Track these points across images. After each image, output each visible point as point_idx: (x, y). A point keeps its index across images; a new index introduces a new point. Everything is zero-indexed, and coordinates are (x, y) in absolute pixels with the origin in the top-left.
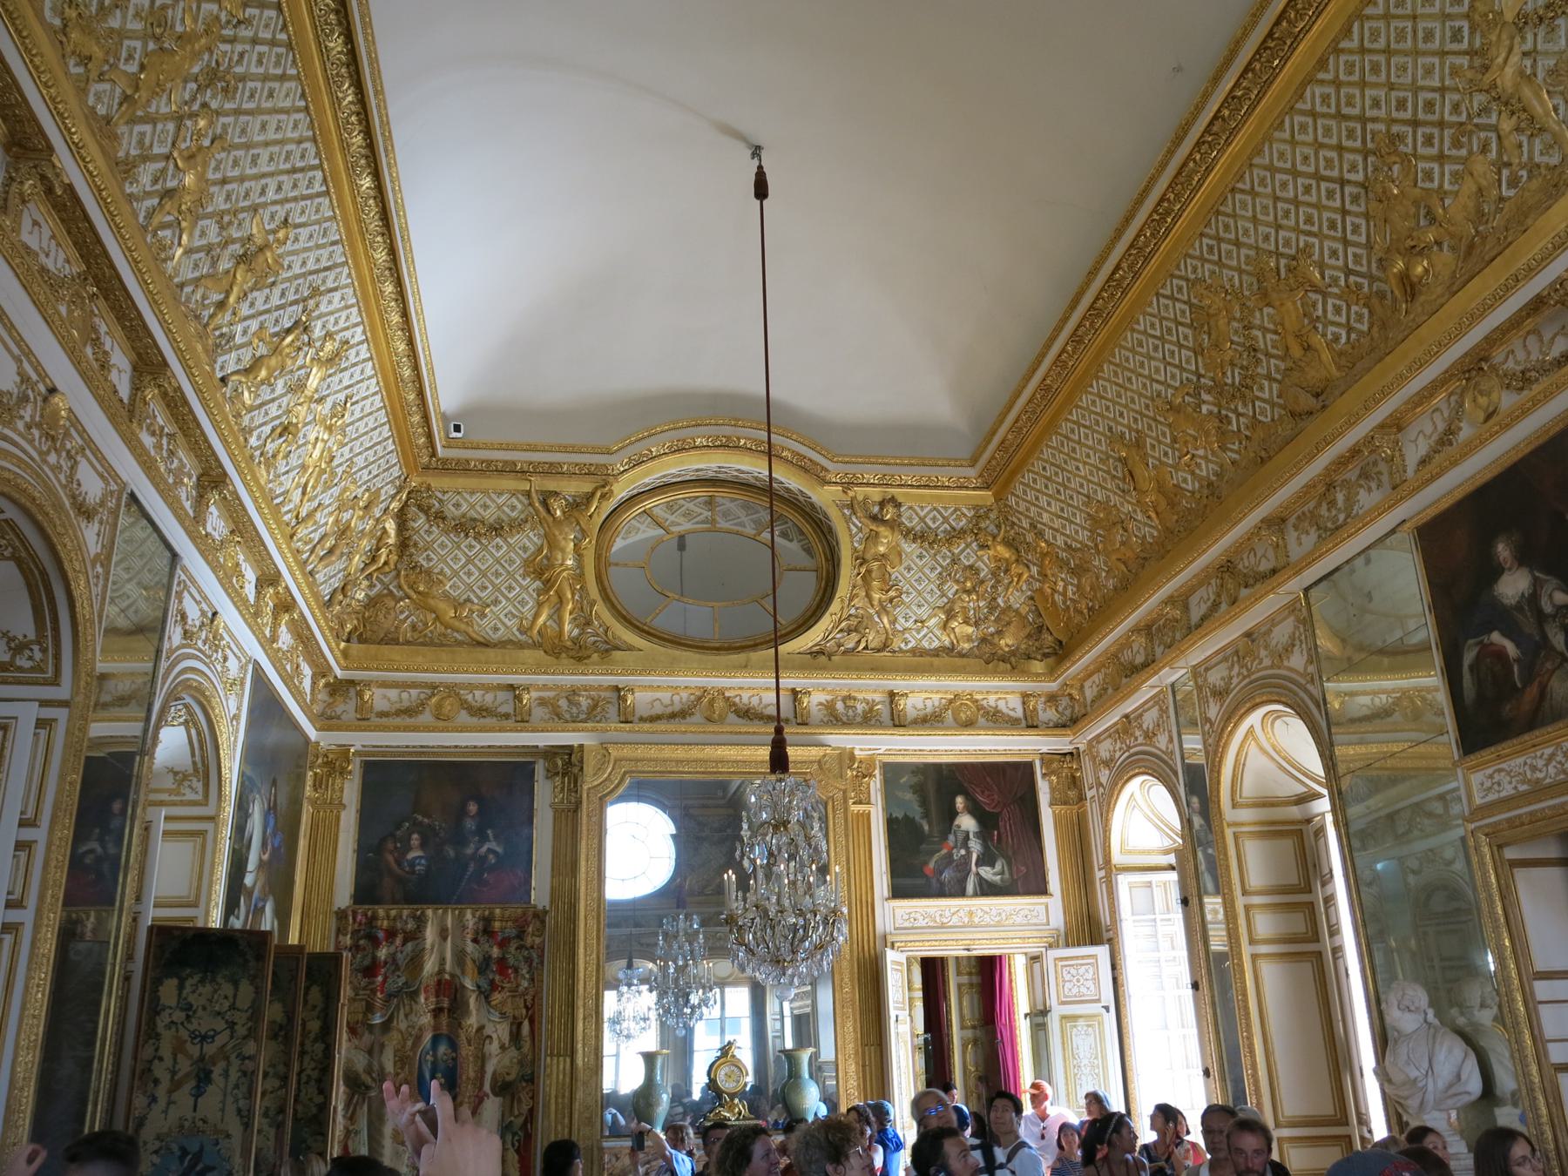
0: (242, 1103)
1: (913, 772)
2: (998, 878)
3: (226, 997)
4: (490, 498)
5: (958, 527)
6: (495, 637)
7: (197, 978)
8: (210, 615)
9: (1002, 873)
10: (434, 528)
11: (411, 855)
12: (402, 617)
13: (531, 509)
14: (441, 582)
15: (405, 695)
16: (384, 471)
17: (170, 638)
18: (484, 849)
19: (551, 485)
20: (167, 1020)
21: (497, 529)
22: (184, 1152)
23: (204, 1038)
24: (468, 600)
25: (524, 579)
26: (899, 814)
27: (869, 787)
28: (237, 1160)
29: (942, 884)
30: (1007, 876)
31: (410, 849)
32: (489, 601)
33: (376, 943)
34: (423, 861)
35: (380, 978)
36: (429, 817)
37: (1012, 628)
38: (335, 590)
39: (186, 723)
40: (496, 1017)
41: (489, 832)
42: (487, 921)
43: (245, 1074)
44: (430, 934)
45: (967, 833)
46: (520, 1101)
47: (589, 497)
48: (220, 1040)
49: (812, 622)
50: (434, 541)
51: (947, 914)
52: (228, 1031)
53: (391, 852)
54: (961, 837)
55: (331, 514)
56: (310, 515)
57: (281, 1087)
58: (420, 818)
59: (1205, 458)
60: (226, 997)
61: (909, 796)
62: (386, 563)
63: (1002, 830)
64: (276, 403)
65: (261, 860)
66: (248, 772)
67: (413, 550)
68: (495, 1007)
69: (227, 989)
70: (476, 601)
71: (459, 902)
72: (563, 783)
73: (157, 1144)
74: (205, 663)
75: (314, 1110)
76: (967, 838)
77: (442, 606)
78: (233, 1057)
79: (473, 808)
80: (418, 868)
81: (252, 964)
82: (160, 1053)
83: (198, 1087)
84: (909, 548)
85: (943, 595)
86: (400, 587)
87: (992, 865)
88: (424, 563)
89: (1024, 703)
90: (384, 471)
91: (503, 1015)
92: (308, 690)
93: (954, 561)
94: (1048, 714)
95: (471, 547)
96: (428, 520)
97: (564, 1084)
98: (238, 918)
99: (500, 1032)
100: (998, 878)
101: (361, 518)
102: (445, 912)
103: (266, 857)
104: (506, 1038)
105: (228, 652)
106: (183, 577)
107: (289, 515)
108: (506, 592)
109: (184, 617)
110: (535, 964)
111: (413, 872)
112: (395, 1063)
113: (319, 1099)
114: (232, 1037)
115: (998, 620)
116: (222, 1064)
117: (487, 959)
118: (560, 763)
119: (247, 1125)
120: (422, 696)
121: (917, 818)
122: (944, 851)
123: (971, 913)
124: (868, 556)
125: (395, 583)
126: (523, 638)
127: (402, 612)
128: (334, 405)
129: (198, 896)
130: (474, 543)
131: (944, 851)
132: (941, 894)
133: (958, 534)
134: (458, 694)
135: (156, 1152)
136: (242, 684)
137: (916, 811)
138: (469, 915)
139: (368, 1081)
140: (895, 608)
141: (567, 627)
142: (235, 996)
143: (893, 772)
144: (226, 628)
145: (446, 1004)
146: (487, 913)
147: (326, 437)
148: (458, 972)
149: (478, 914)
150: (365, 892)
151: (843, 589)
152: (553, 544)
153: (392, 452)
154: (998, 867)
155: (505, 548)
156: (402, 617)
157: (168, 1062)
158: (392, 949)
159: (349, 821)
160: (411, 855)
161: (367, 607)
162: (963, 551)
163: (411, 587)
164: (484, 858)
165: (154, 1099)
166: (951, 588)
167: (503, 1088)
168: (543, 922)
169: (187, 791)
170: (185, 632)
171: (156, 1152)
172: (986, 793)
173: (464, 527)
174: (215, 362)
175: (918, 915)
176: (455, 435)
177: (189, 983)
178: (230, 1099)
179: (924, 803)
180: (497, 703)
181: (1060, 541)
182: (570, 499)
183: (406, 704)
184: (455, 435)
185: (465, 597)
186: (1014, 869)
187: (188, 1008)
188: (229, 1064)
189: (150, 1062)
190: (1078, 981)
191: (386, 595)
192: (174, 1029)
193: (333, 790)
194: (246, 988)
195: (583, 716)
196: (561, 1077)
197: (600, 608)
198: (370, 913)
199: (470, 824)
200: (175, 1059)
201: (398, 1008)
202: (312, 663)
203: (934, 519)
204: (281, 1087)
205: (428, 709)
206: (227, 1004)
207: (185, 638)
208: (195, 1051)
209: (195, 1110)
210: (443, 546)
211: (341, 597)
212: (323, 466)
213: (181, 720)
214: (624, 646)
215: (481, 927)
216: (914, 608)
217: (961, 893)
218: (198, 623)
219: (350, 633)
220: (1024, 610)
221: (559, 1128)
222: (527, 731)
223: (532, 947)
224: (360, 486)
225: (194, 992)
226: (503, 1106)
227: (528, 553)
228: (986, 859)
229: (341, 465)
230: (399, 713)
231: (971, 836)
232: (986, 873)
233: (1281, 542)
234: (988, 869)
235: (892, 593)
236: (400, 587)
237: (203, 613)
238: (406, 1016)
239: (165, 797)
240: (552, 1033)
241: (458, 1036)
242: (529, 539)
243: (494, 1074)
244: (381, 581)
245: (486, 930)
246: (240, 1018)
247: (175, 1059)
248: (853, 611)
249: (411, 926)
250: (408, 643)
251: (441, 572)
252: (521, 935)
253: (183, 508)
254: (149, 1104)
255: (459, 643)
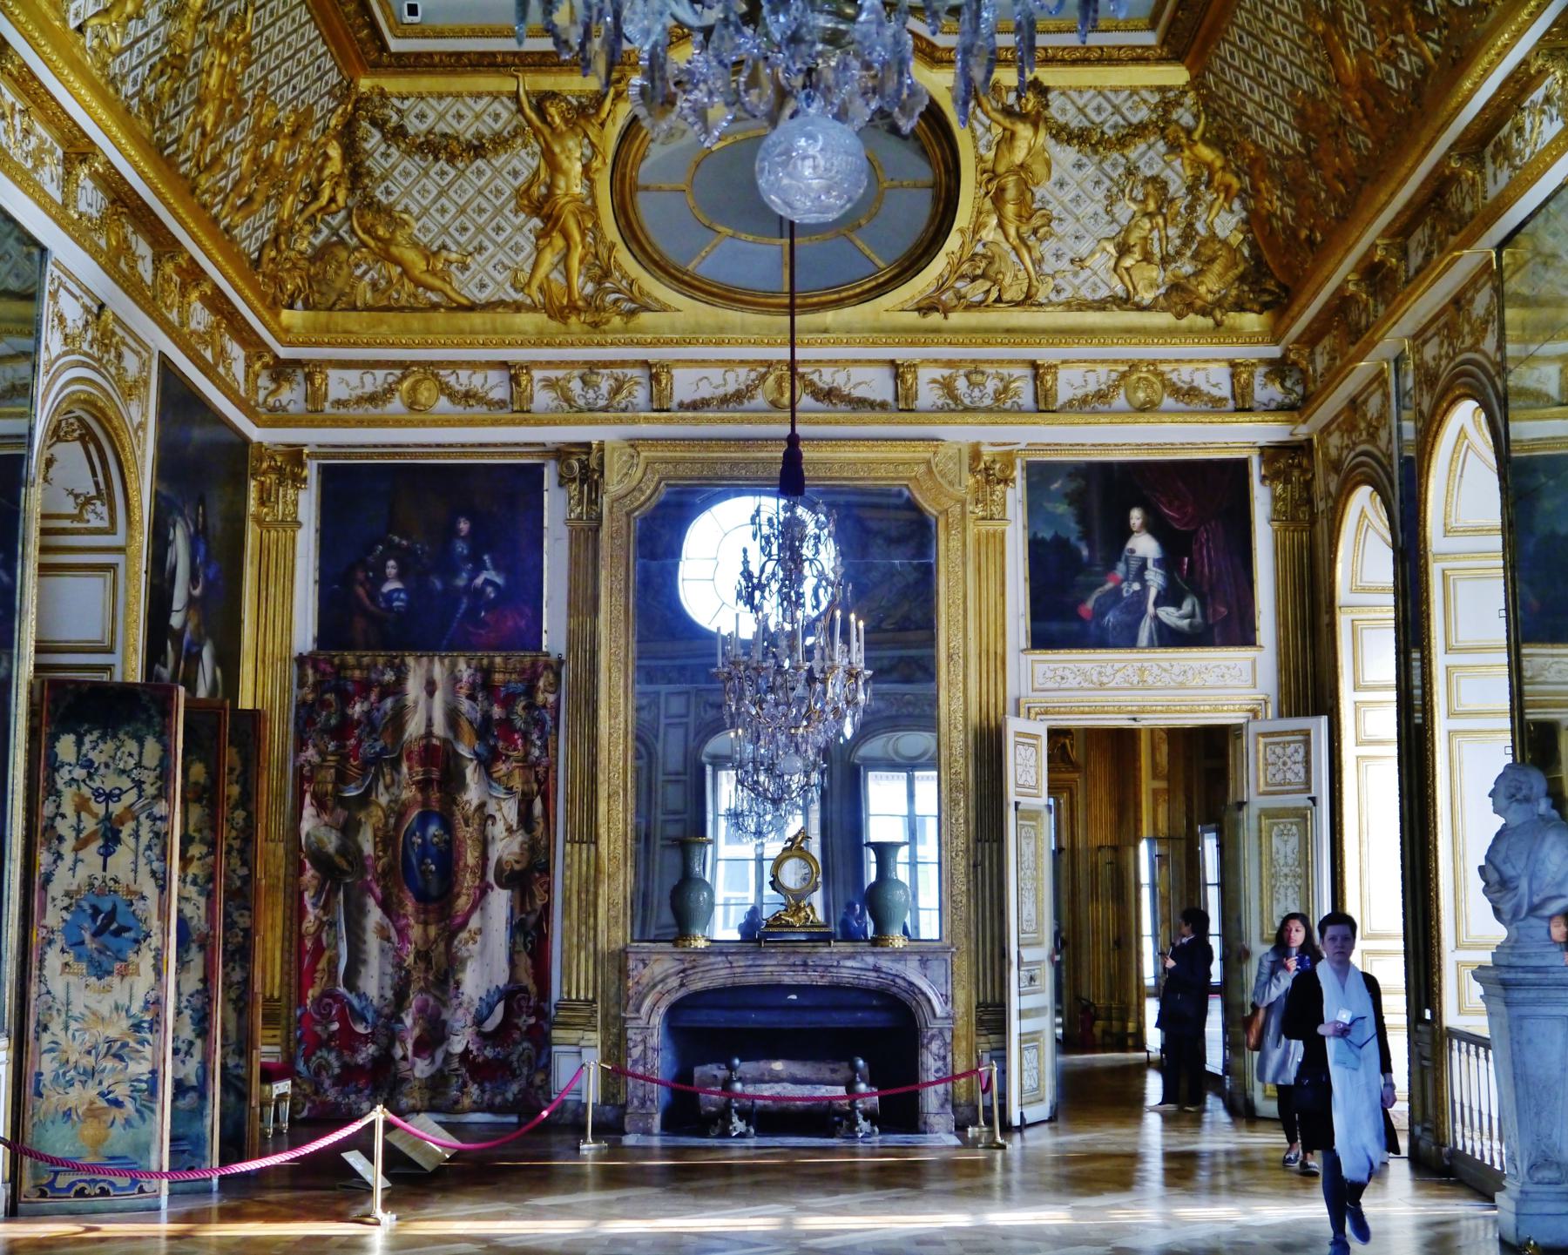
0: (156, 865)
1: (1070, 475)
2: (1187, 621)
3: (130, 755)
4: (465, 104)
5: (1135, 121)
6: (482, 297)
7: (96, 734)
8: (95, 309)
9: (1192, 616)
10: (393, 150)
11: (388, 587)
12: (358, 272)
13: (520, 117)
14: (406, 223)
15: (368, 378)
16: (315, 81)
17: (47, 347)
18: (479, 581)
19: (547, 82)
20: (67, 777)
21: (477, 149)
22: (96, 911)
23: (109, 797)
24: (444, 247)
25: (516, 215)
26: (1046, 534)
27: (1004, 497)
28: (155, 923)
29: (1104, 629)
30: (1198, 619)
31: (385, 579)
32: (470, 249)
33: (346, 699)
34: (402, 596)
35: (353, 742)
36: (407, 538)
37: (1217, 267)
38: (264, 245)
39: (81, 438)
40: (500, 793)
41: (486, 557)
42: (487, 672)
43: (157, 835)
44: (414, 688)
45: (1144, 561)
46: (532, 896)
47: (599, 99)
48: (130, 798)
49: (922, 263)
50: (393, 167)
51: (1109, 671)
52: (135, 791)
53: (362, 584)
54: (1134, 565)
55: (244, 152)
56: (216, 158)
57: (208, 854)
58: (396, 539)
59: (1405, 46)
60: (130, 755)
61: (1062, 508)
62: (332, 200)
63: (1196, 557)
64: (152, 36)
65: (190, 595)
66: (164, 492)
67: (367, 181)
68: (498, 780)
69: (132, 746)
70: (454, 248)
71: (450, 648)
72: (581, 492)
73: (67, 902)
74: (94, 369)
75: (238, 883)
76: (1143, 566)
77: (411, 256)
78: (143, 817)
79: (464, 526)
80: (396, 604)
81: (157, 720)
82: (62, 810)
83: (105, 846)
84: (1065, 155)
85: (1113, 221)
86: (352, 232)
87: (1178, 605)
88: (383, 198)
89: (1233, 376)
90: (315, 81)
91: (509, 790)
92: (240, 376)
93: (1130, 172)
94: (1266, 391)
95: (443, 173)
96: (385, 138)
97: (587, 879)
98: (165, 666)
99: (505, 810)
100: (1187, 621)
101: (291, 149)
102: (431, 662)
103: (197, 592)
104: (513, 818)
105: (125, 350)
106: (57, 272)
107: (188, 165)
108: (493, 235)
109: (61, 319)
110: (542, 723)
111: (390, 609)
112: (376, 844)
113: (244, 871)
114: (140, 797)
115: (1195, 256)
116: (131, 825)
117: (487, 717)
118: (576, 465)
119: (163, 886)
120: (391, 379)
121: (1073, 539)
122: (1109, 585)
123: (1142, 670)
124: (1001, 169)
125: (345, 227)
126: (519, 297)
127: (358, 266)
128: (232, 17)
129: (113, 641)
130: (447, 168)
131: (1109, 585)
132: (1102, 643)
133: (1140, 130)
134: (436, 376)
135: (66, 909)
136: (146, 383)
137: (1072, 530)
138: (462, 665)
139: (344, 865)
140: (1041, 241)
141: (577, 281)
142: (141, 754)
143: (1040, 475)
144: (117, 319)
145: (436, 775)
146: (485, 662)
147: (224, 60)
148: (450, 736)
149: (474, 663)
150: (331, 630)
151: (963, 217)
152: (554, 166)
153: (324, 54)
154: (1187, 606)
155: (489, 173)
156: (358, 272)
157: (72, 819)
158: (366, 706)
159: (306, 542)
160: (388, 587)
161: (312, 260)
162: (1143, 155)
163: (367, 231)
164: (480, 592)
165: (59, 856)
166: (1126, 209)
167: (509, 879)
168: (558, 675)
169: (91, 517)
170: (66, 337)
171: (66, 909)
172: (1176, 503)
173: (435, 147)
174: (67, 11)
175: (1067, 672)
176: (408, 19)
177: (88, 739)
178: (142, 861)
179: (1083, 519)
180: (487, 387)
181: (1270, 143)
182: (575, 102)
183: (369, 389)
184: (408, 19)
185: (439, 243)
186: (1210, 611)
187: (88, 764)
188: (139, 824)
189: (53, 819)
190: (1284, 764)
191: (334, 244)
192: (75, 787)
193: (285, 502)
194: (152, 748)
195: (602, 403)
196: (584, 868)
197: (623, 256)
198: (337, 661)
199: (461, 548)
200: (79, 817)
201: (376, 779)
202: (244, 343)
203: (1099, 110)
204: (208, 854)
205: (397, 394)
206: (132, 762)
207: (66, 344)
208: (100, 809)
209: (104, 869)
210: (406, 174)
211: (273, 254)
212: (225, 95)
213: (76, 434)
214: (657, 307)
215: (479, 680)
216: (1071, 241)
217: (1130, 642)
218: (80, 323)
219: (292, 296)
220: (1236, 239)
221: (583, 929)
222: (528, 424)
223: (544, 706)
224: (283, 108)
225: (94, 748)
226: (512, 900)
227: (521, 179)
228: (1170, 596)
229: (251, 88)
230: (360, 400)
231: (1150, 564)
232: (1169, 615)
233: (1478, 177)
234: (1171, 610)
235: (1036, 222)
236: (352, 232)
237: (87, 309)
238: (387, 788)
239: (67, 524)
240: (572, 815)
241: (452, 814)
242: (523, 161)
243: (499, 861)
244: (328, 225)
245: (484, 685)
246: (148, 777)
247: (79, 817)
248: (979, 249)
249: (389, 676)
250: (368, 308)
251: (406, 210)
252: (531, 690)
253: (46, 195)
254: (55, 862)
255: (435, 307)
